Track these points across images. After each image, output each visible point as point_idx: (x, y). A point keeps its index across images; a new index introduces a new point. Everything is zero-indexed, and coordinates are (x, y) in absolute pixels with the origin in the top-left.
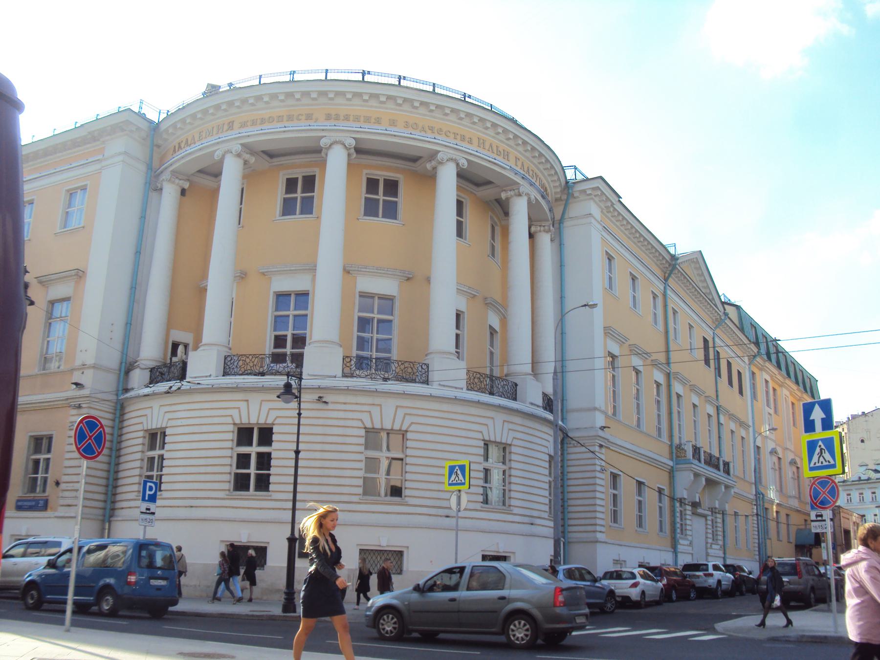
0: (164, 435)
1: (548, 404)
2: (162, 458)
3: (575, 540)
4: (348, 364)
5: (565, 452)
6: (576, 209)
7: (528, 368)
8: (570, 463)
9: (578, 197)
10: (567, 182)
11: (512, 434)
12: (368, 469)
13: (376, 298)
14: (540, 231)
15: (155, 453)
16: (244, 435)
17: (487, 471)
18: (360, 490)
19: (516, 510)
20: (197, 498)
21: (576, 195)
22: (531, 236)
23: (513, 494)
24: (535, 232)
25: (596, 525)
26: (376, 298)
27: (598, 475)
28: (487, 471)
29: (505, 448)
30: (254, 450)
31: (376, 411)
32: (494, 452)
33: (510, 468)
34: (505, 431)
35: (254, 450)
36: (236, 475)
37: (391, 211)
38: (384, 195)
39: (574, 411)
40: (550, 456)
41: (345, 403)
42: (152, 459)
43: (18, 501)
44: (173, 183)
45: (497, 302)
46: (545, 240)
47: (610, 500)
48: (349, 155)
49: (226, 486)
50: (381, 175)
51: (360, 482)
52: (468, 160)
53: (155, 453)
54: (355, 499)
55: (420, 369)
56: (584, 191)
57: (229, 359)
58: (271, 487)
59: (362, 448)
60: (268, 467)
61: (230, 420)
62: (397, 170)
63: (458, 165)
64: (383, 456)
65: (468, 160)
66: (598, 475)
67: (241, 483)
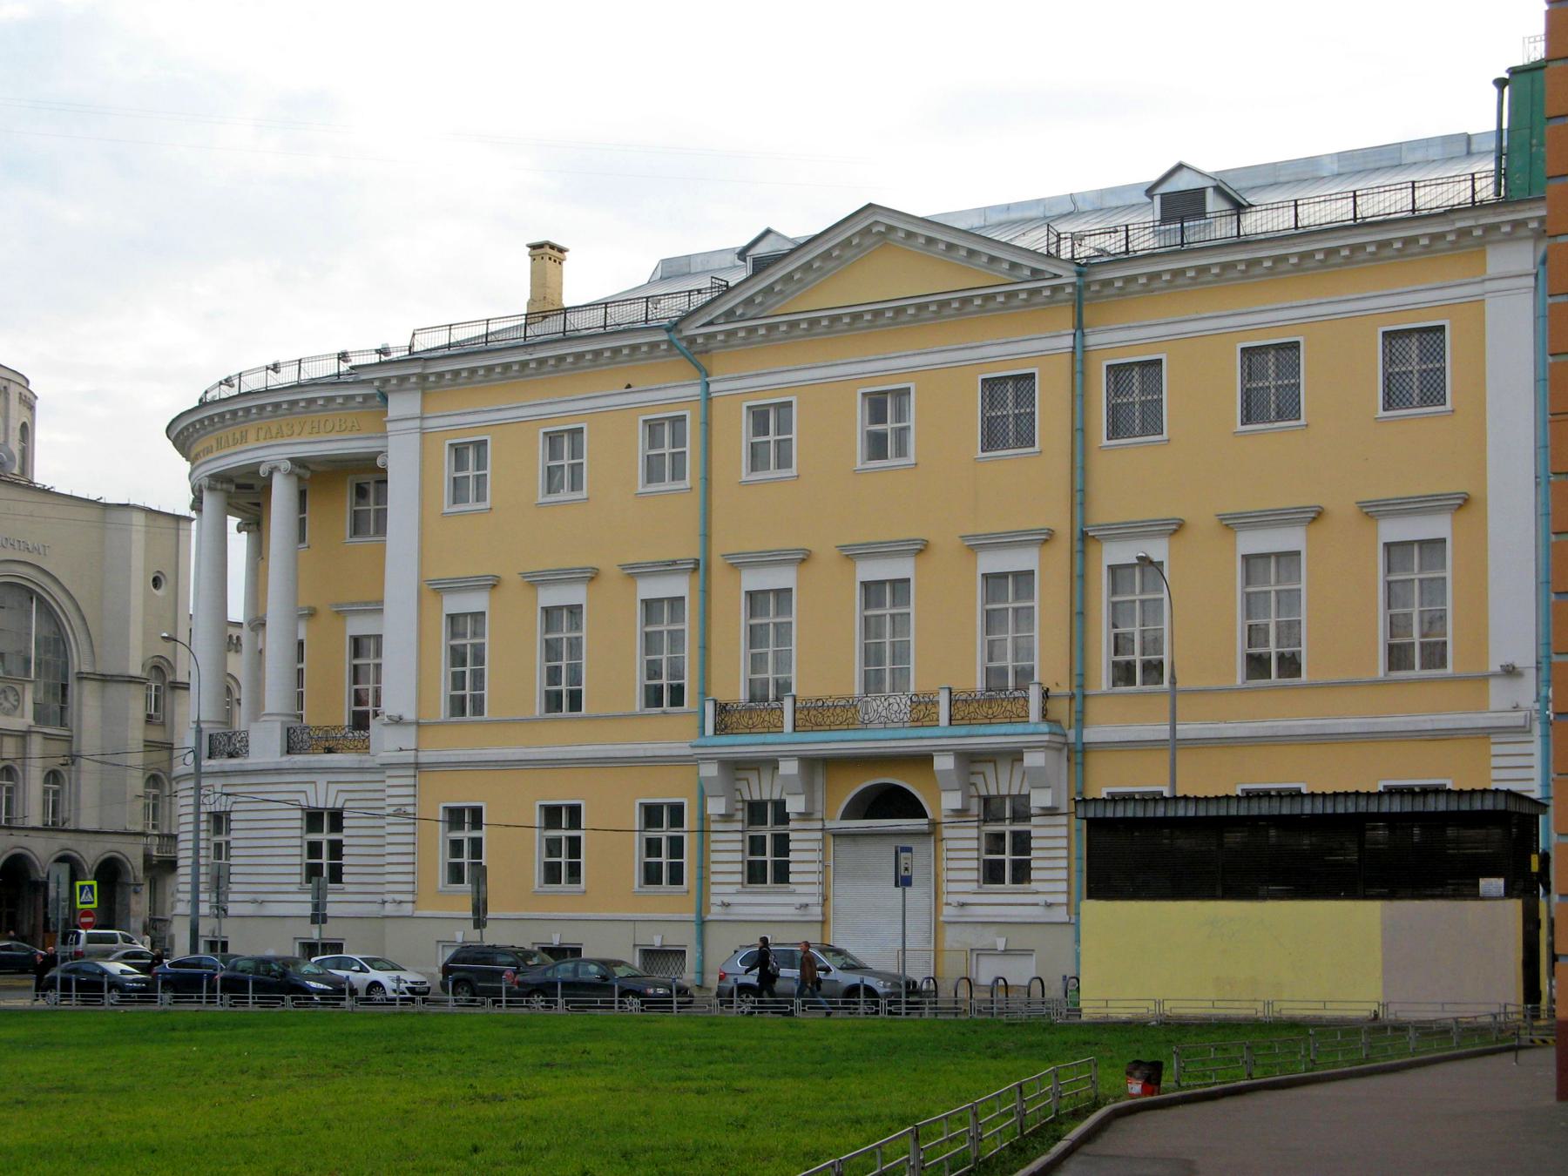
0: (229, 821)
2: (228, 843)
15: (221, 839)
19: (349, 888)
30: (768, 831)
35: (324, 837)
36: (308, 865)
42: (218, 846)
49: (297, 879)
53: (221, 839)
54: (294, 888)
58: (792, 878)
59: (792, 836)
60: (1027, 850)
67: (652, 875)
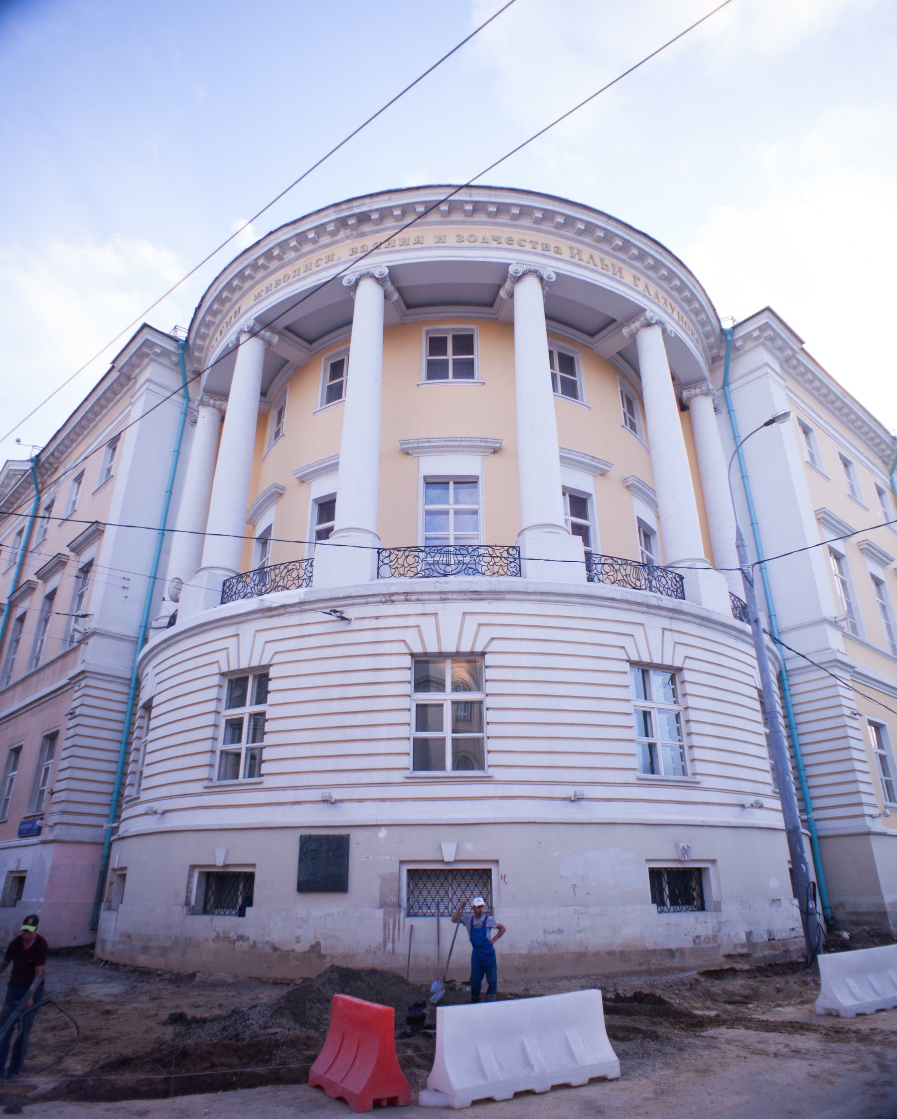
1: (743, 611)
3: (829, 833)
4: (386, 561)
5: (788, 693)
6: (743, 366)
7: (700, 552)
8: (800, 719)
9: (743, 347)
10: (722, 330)
11: (681, 651)
12: (422, 725)
13: (451, 485)
14: (696, 396)
17: (646, 715)
18: (408, 761)
20: (171, 797)
21: (739, 343)
22: (684, 407)
23: (698, 754)
24: (690, 398)
25: (861, 804)
26: (451, 485)
27: (848, 722)
28: (646, 715)
29: (674, 673)
31: (428, 624)
32: (657, 680)
33: (686, 708)
34: (668, 647)
37: (466, 370)
38: (454, 354)
39: (790, 630)
40: (759, 691)
41: (377, 618)
43: (22, 823)
44: (208, 405)
45: (644, 484)
46: (703, 407)
47: (877, 762)
48: (386, 297)
50: (449, 328)
51: (408, 747)
52: (556, 273)
54: (397, 777)
55: (505, 554)
56: (748, 337)
57: (228, 584)
61: (214, 669)
62: (468, 320)
63: (541, 279)
64: (446, 698)
65: (556, 273)
66: (848, 722)
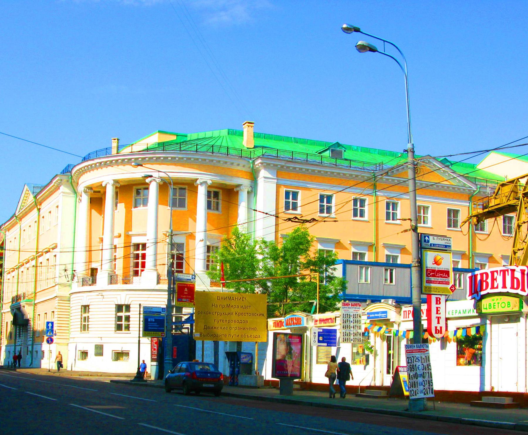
16: (119, 308)
67: (119, 327)
